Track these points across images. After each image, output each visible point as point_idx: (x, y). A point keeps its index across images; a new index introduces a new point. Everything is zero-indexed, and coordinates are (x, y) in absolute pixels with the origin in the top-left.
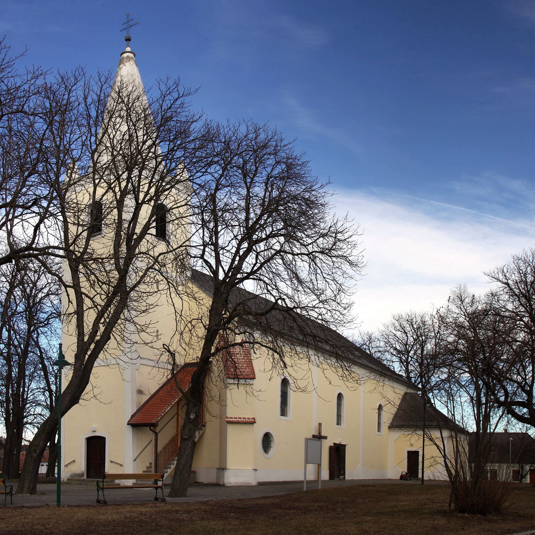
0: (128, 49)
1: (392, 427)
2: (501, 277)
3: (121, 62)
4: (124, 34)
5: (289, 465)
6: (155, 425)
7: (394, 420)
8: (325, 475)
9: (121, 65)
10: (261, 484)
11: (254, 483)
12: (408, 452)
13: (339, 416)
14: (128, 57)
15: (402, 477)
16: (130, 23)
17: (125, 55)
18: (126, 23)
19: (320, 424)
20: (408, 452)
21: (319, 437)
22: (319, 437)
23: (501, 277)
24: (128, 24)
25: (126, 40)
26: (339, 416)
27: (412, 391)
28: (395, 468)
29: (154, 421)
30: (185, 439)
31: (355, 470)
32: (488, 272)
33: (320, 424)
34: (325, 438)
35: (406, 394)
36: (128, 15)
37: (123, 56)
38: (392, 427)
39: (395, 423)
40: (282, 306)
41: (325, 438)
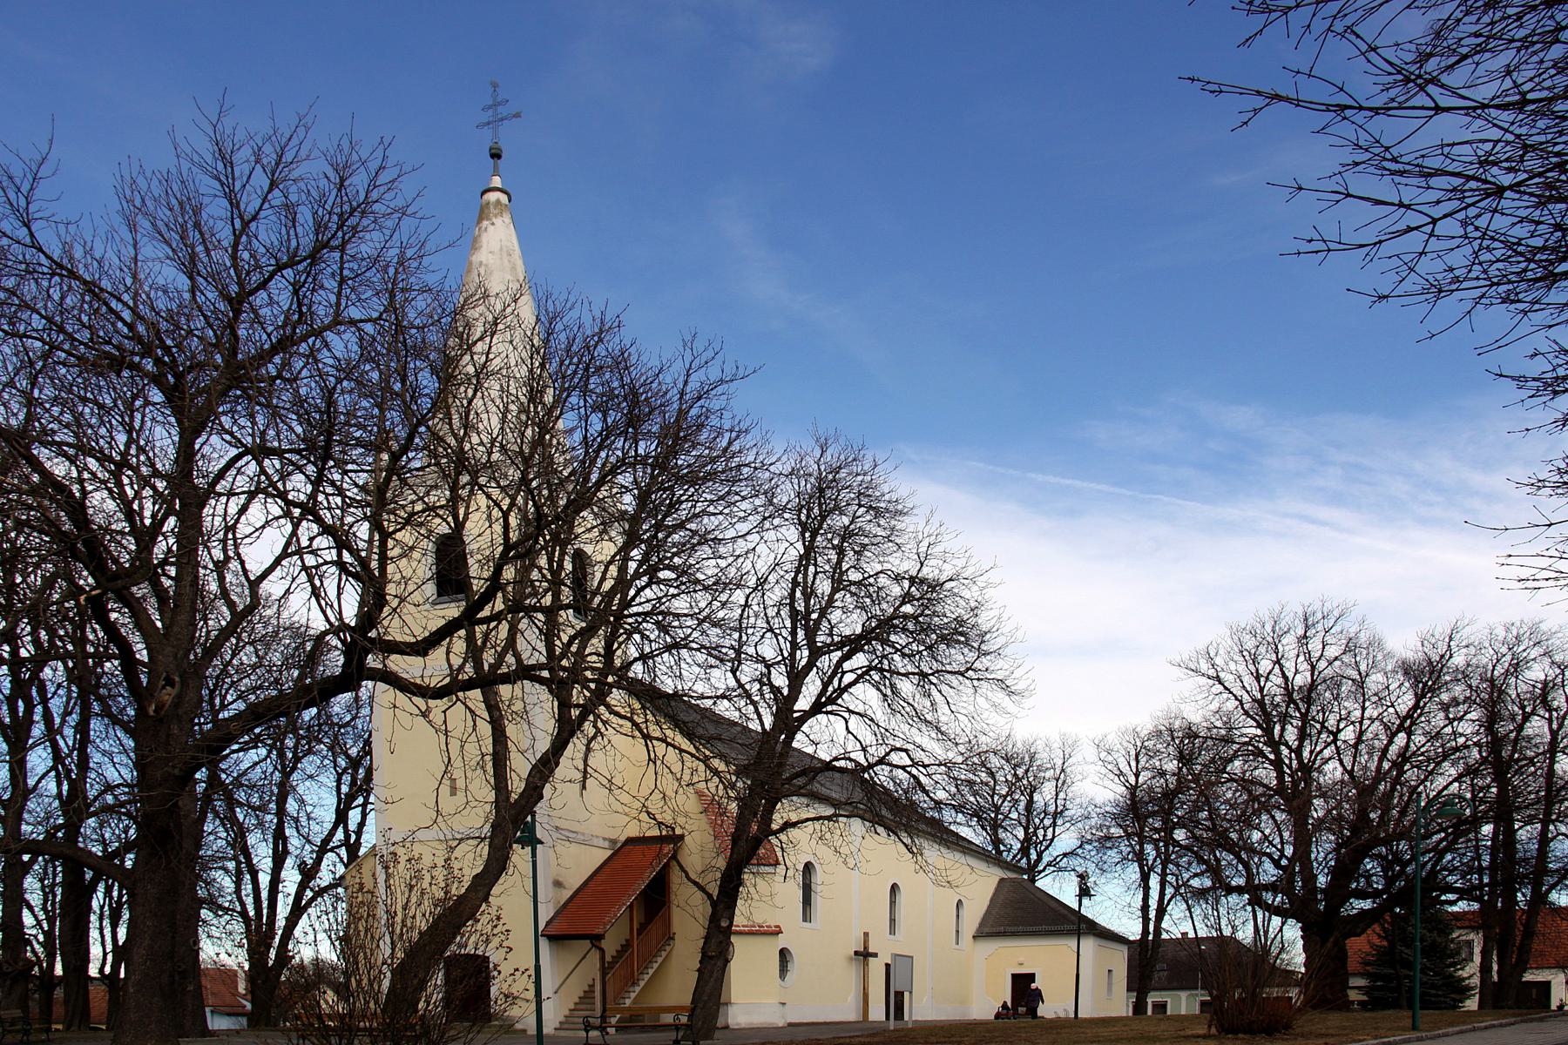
0: (497, 182)
1: (983, 933)
2: (1204, 666)
3: (483, 214)
4: (486, 140)
5: (829, 996)
6: (600, 937)
7: (982, 924)
8: (877, 1013)
9: (485, 223)
10: (790, 1025)
11: (781, 1024)
12: (1014, 976)
13: (893, 921)
14: (498, 202)
15: (998, 1016)
16: (500, 109)
17: (492, 197)
18: (490, 107)
19: (866, 935)
20: (1014, 976)
21: (864, 955)
22: (864, 955)
23: (1204, 666)
24: (497, 113)
25: (493, 156)
26: (893, 921)
27: (1013, 875)
28: (984, 1000)
29: (597, 931)
30: (711, 958)
31: (1054, 1006)
32: (1178, 659)
33: (866, 935)
34: (875, 955)
35: (1002, 880)
36: (495, 86)
37: (486, 197)
38: (983, 933)
39: (986, 930)
40: (29, 737)
41: (875, 955)
